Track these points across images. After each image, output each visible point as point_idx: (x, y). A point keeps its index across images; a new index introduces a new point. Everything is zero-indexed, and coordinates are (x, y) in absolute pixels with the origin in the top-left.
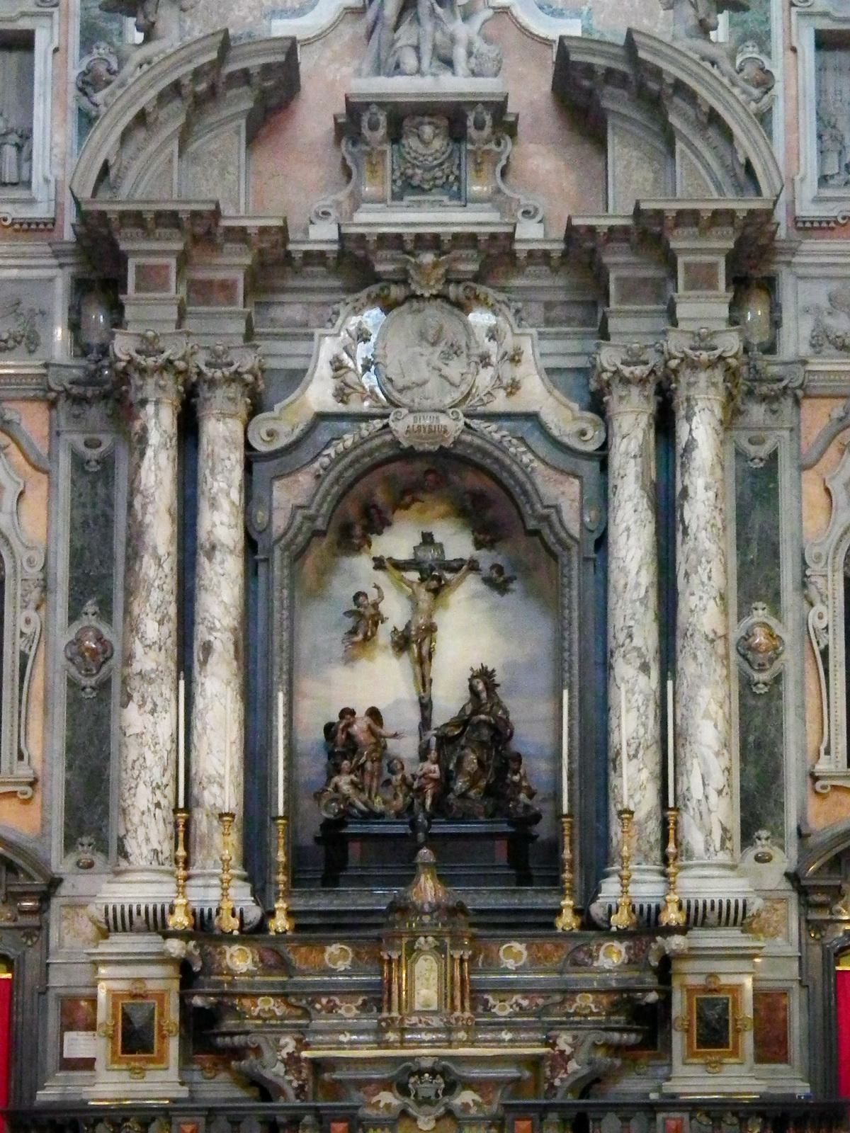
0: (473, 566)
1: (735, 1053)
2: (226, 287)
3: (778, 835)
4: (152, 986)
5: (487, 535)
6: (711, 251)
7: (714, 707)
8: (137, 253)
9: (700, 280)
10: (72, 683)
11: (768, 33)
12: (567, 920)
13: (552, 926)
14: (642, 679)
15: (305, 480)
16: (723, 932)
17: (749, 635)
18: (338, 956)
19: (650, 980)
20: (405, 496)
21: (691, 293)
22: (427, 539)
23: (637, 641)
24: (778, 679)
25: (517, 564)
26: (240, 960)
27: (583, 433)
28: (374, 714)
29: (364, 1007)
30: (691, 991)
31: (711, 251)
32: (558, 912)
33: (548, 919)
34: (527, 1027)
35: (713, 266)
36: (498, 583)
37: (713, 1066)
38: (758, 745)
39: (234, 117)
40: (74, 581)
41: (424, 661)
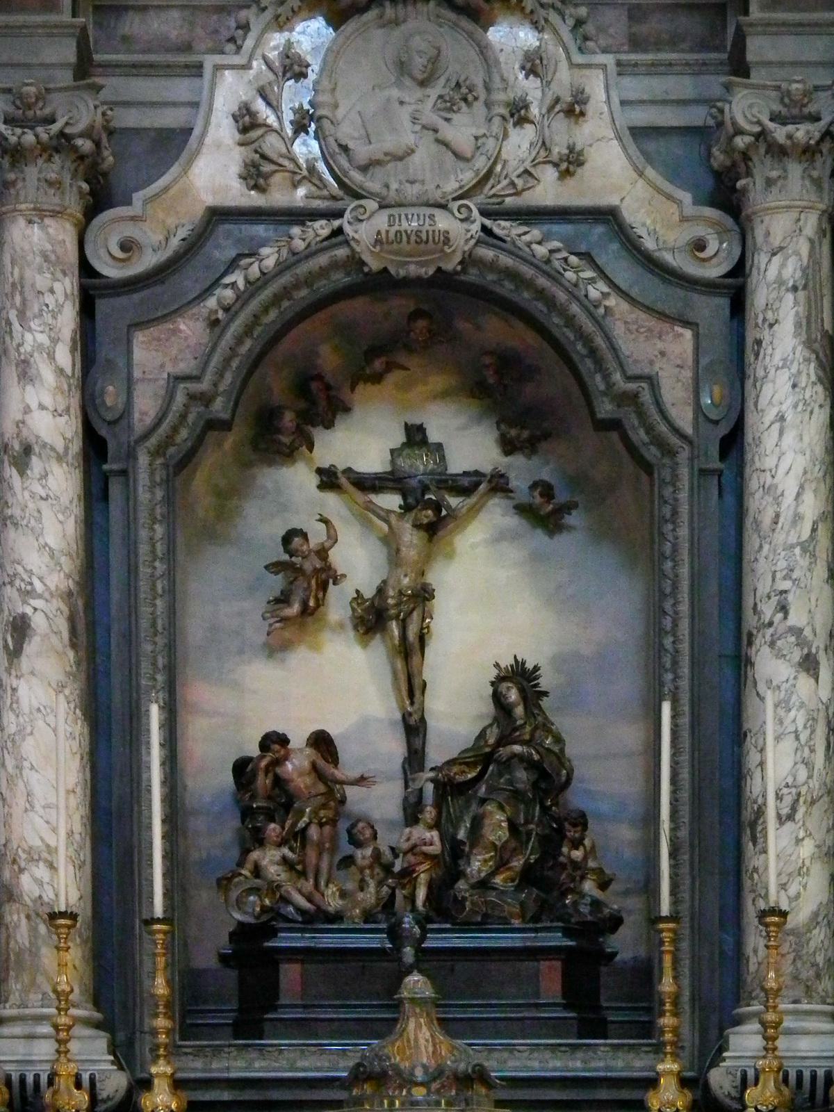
0: (498, 484)
15: (191, 329)
22: (416, 436)
23: (797, 617)
25: (577, 481)
27: (700, 245)
28: (322, 742)
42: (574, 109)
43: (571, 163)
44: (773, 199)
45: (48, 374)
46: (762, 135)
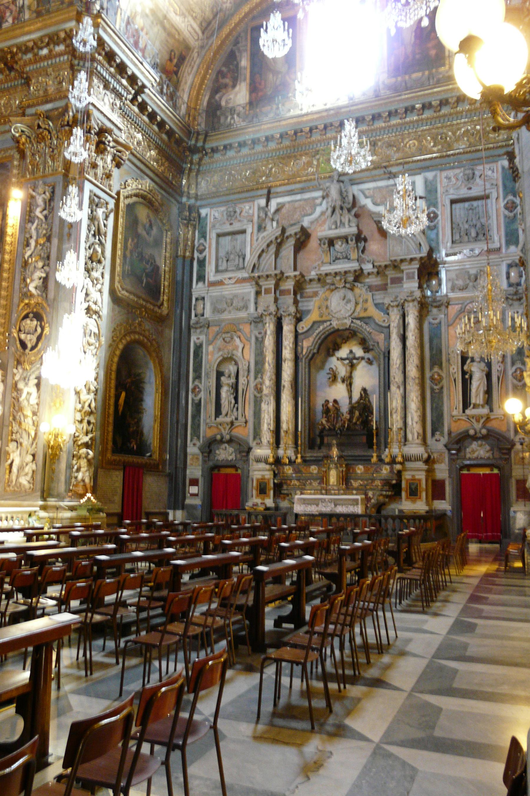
0: (363, 358)
1: (420, 498)
2: (288, 291)
3: (442, 434)
4: (267, 477)
5: (367, 350)
6: (414, 268)
7: (415, 398)
8: (264, 285)
9: (410, 277)
10: (255, 396)
11: (437, 202)
12: (374, 459)
13: (370, 460)
14: (398, 391)
15: (311, 339)
16: (417, 463)
17: (433, 375)
18: (314, 469)
19: (395, 477)
20: (346, 340)
21: (393, 285)
22: (351, 352)
23: (397, 380)
24: (442, 388)
25: (374, 357)
26: (289, 470)
27: (384, 321)
28: (335, 401)
29: (319, 483)
30: (407, 480)
31: (414, 268)
32: (372, 457)
33: (369, 458)
34: (361, 490)
35: (413, 273)
36: (370, 362)
37: (414, 502)
38: (437, 408)
39: (290, 246)
40: (256, 370)
41: (350, 384)
42: (366, 301)
43: (366, 310)
44: (409, 309)
45: (288, 348)
46: (389, 305)
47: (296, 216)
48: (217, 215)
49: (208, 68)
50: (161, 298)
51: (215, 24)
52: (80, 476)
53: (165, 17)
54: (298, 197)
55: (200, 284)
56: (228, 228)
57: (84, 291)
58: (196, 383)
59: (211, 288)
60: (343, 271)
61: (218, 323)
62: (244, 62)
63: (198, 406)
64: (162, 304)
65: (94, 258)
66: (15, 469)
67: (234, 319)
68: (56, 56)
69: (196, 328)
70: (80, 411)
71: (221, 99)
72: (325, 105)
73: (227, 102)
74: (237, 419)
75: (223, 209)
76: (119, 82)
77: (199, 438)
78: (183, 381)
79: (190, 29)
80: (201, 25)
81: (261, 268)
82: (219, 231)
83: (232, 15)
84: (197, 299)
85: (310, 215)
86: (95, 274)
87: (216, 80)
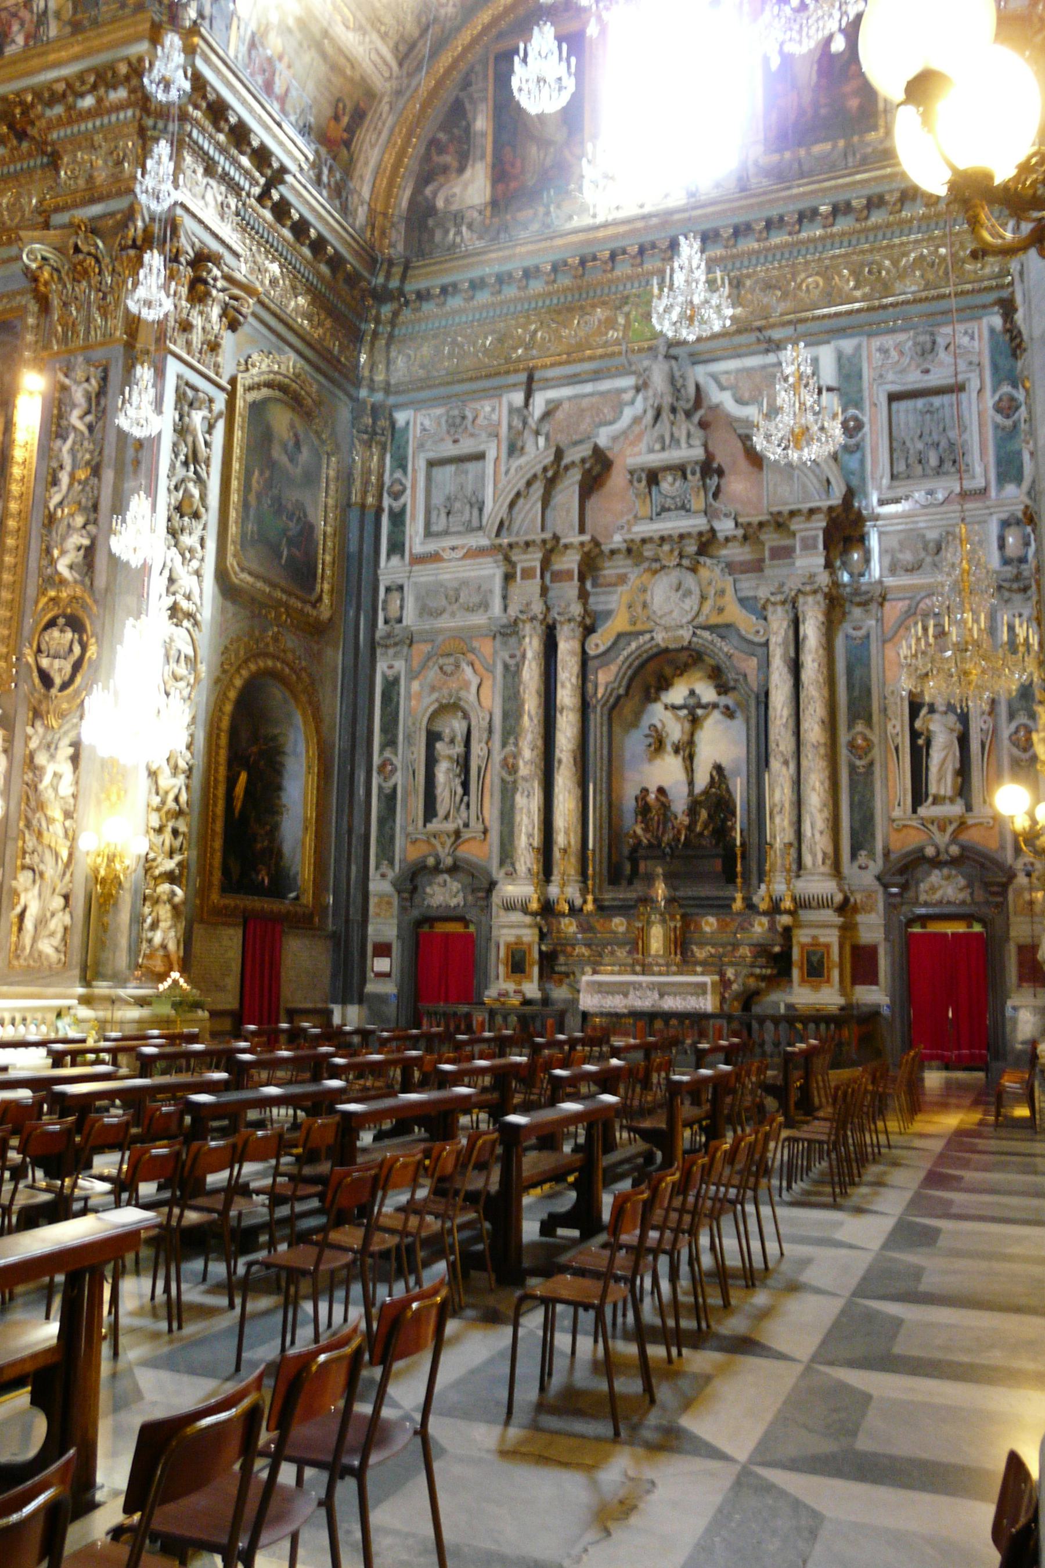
0: (715, 706)
1: (828, 981)
2: (569, 573)
3: (872, 854)
4: (526, 939)
5: (723, 689)
6: (816, 529)
7: (817, 784)
8: (521, 561)
9: (808, 546)
10: (503, 780)
11: (862, 399)
12: (738, 905)
13: (729, 907)
14: (784, 769)
15: (614, 668)
16: (822, 912)
17: (854, 739)
18: (619, 924)
19: (779, 940)
20: (682, 670)
21: (775, 562)
22: (692, 693)
23: (782, 748)
24: (871, 764)
25: (738, 704)
26: (569, 926)
27: (758, 632)
28: (661, 791)
29: (630, 952)
30: (803, 946)
31: (816, 529)
32: (734, 899)
33: (727, 902)
34: (712, 964)
35: (815, 538)
36: (729, 713)
37: (816, 988)
38: (861, 803)
39: (573, 484)
40: (504, 728)
41: (691, 757)
42: (722, 593)
43: (721, 610)
44: (806, 608)
45: (568, 685)
46: (768, 600)
47: (584, 426)
48: (427, 423)
49: (410, 134)
50: (318, 587)
51: (425, 48)
52: (158, 937)
53: (326, 34)
54: (588, 388)
55: (395, 560)
56: (449, 450)
57: (166, 573)
58: (387, 754)
59: (416, 568)
60: (675, 533)
61: (430, 637)
62: (482, 123)
63: (390, 799)
64: (320, 599)
65: (186, 509)
66: (29, 924)
67: (461, 629)
68: (110, 111)
69: (386, 646)
70: (158, 810)
71: (435, 194)
72: (642, 206)
73: (447, 201)
74: (466, 825)
75: (439, 411)
76: (235, 162)
77: (391, 862)
78: (360, 751)
79: (374, 56)
80: (396, 50)
81: (515, 527)
82: (432, 455)
83: (458, 29)
84: (388, 590)
85: (611, 423)
86: (187, 540)
87: (427, 158)
